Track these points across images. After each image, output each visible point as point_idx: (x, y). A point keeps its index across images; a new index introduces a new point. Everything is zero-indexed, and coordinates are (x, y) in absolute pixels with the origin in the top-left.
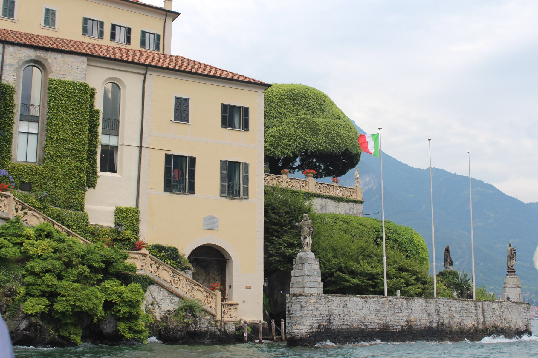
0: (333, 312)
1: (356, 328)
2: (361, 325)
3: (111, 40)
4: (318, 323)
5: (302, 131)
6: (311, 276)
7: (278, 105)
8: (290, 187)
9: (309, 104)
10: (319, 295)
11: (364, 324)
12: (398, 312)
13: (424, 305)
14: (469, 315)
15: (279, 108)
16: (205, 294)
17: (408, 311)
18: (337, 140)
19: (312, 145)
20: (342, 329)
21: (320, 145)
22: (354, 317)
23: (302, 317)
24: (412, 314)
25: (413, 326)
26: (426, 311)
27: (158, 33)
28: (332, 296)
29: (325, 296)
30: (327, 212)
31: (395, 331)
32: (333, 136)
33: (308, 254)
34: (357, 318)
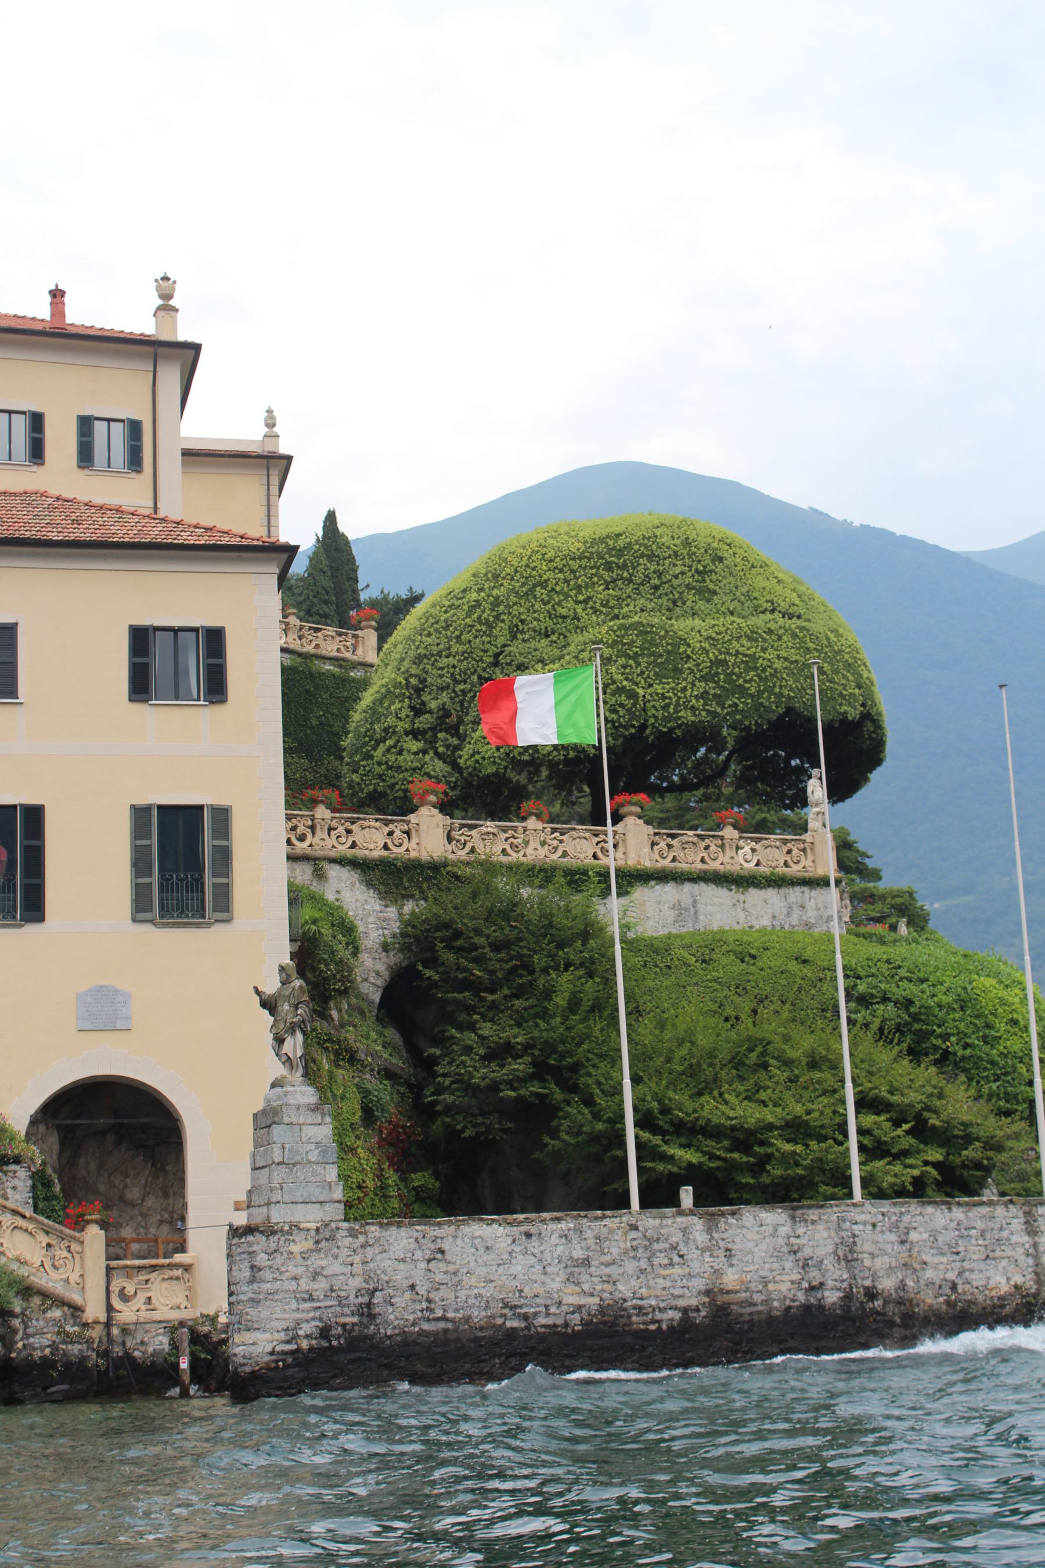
0: (386, 1278)
1: (482, 1329)
2: (504, 1316)
3: (79, 467)
4: (321, 1319)
5: (624, 667)
6: (294, 1165)
7: (556, 592)
8: (555, 857)
9: (660, 574)
10: (327, 1225)
11: (518, 1311)
12: (666, 1261)
13: (784, 1230)
14: (998, 1253)
15: (560, 601)
16: (44, 1239)
17: (711, 1256)
18: (747, 685)
19: (656, 709)
20: (422, 1333)
21: (686, 708)
22: (476, 1291)
23: (255, 1302)
24: (732, 1265)
25: (734, 1307)
26: (795, 1252)
27: (133, 417)
28: (381, 1225)
29: (350, 1230)
30: (700, 926)
31: (653, 1327)
32: (732, 673)
33: (286, 1093)
34: (488, 1292)
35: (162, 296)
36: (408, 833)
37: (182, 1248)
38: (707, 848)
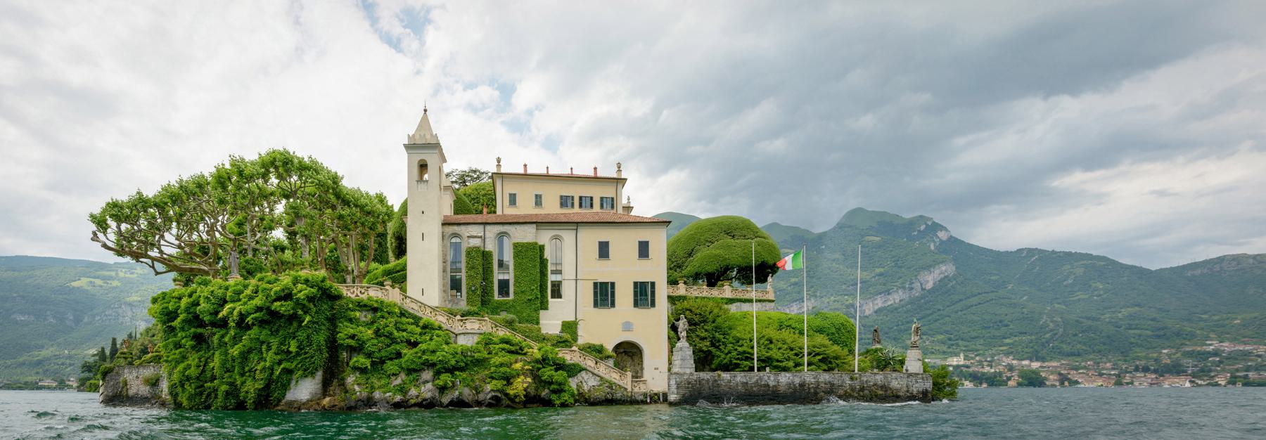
37: (642, 377)
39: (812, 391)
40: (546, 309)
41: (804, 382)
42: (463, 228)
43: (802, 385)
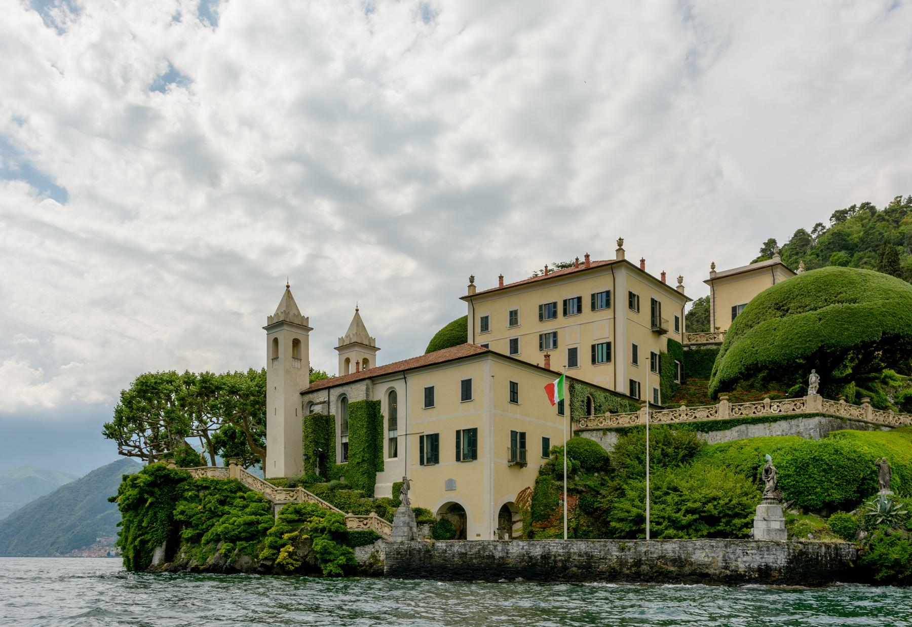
35: (619, 245)
36: (803, 404)
38: (756, 408)
39: (560, 565)
40: (382, 470)
41: (549, 553)
42: (315, 394)
43: (545, 557)
